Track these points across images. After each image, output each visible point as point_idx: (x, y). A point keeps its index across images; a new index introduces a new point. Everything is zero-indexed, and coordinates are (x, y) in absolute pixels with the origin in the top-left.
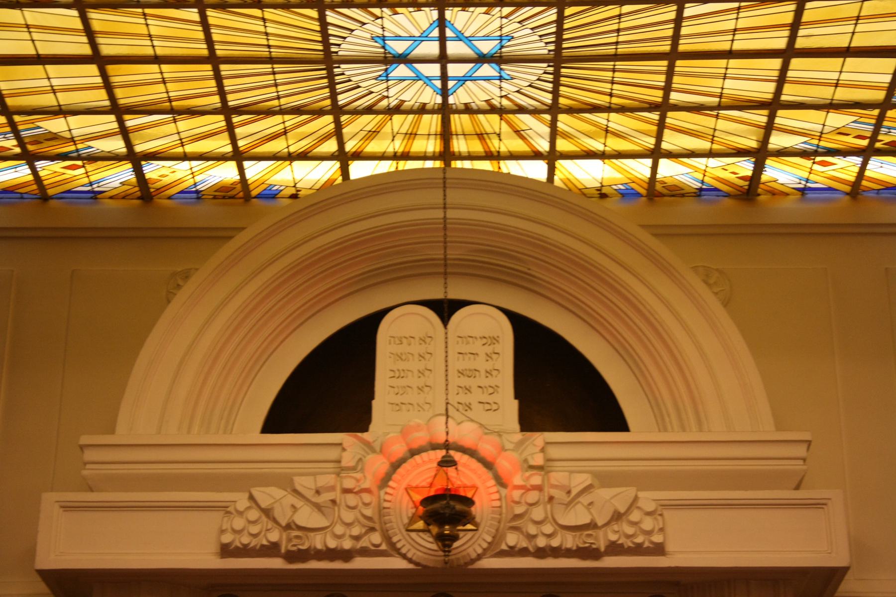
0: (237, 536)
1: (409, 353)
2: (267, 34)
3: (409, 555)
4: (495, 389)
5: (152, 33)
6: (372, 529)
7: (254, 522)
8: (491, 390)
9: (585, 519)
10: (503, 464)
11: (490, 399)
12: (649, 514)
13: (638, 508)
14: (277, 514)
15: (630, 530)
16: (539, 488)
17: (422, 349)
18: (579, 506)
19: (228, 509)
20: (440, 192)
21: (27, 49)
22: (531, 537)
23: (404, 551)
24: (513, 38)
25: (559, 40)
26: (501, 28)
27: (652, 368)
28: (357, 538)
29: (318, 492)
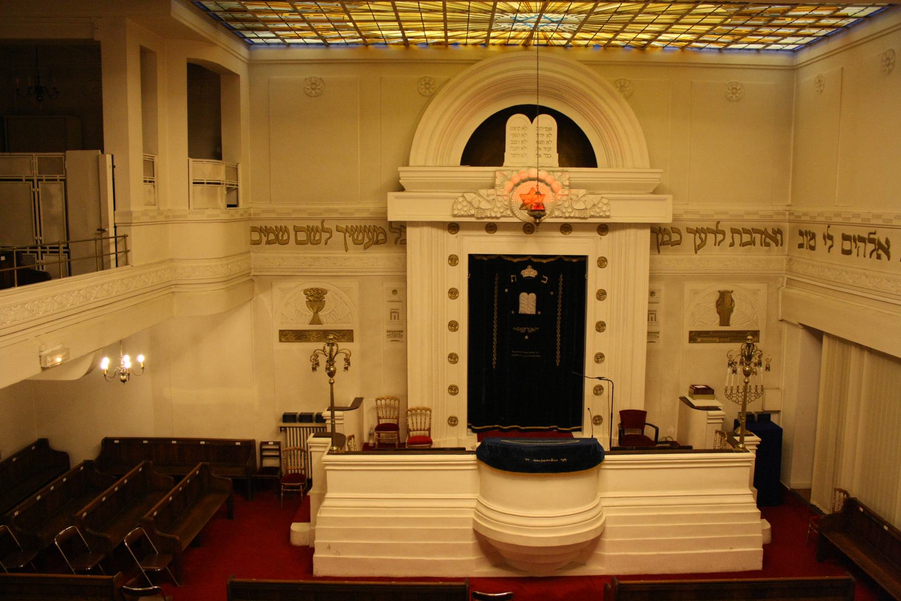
0: (459, 211)
1: (481, 60)
3: (520, 218)
4: (550, 149)
5: (421, 7)
7: (466, 206)
8: (548, 149)
9: (583, 207)
10: (555, 185)
11: (548, 153)
12: (605, 204)
13: (602, 202)
14: (473, 204)
15: (598, 211)
16: (567, 195)
17: (523, 132)
18: (581, 202)
20: (537, 71)
22: (563, 213)
23: (518, 217)
27: (606, 135)
29: (488, 196)
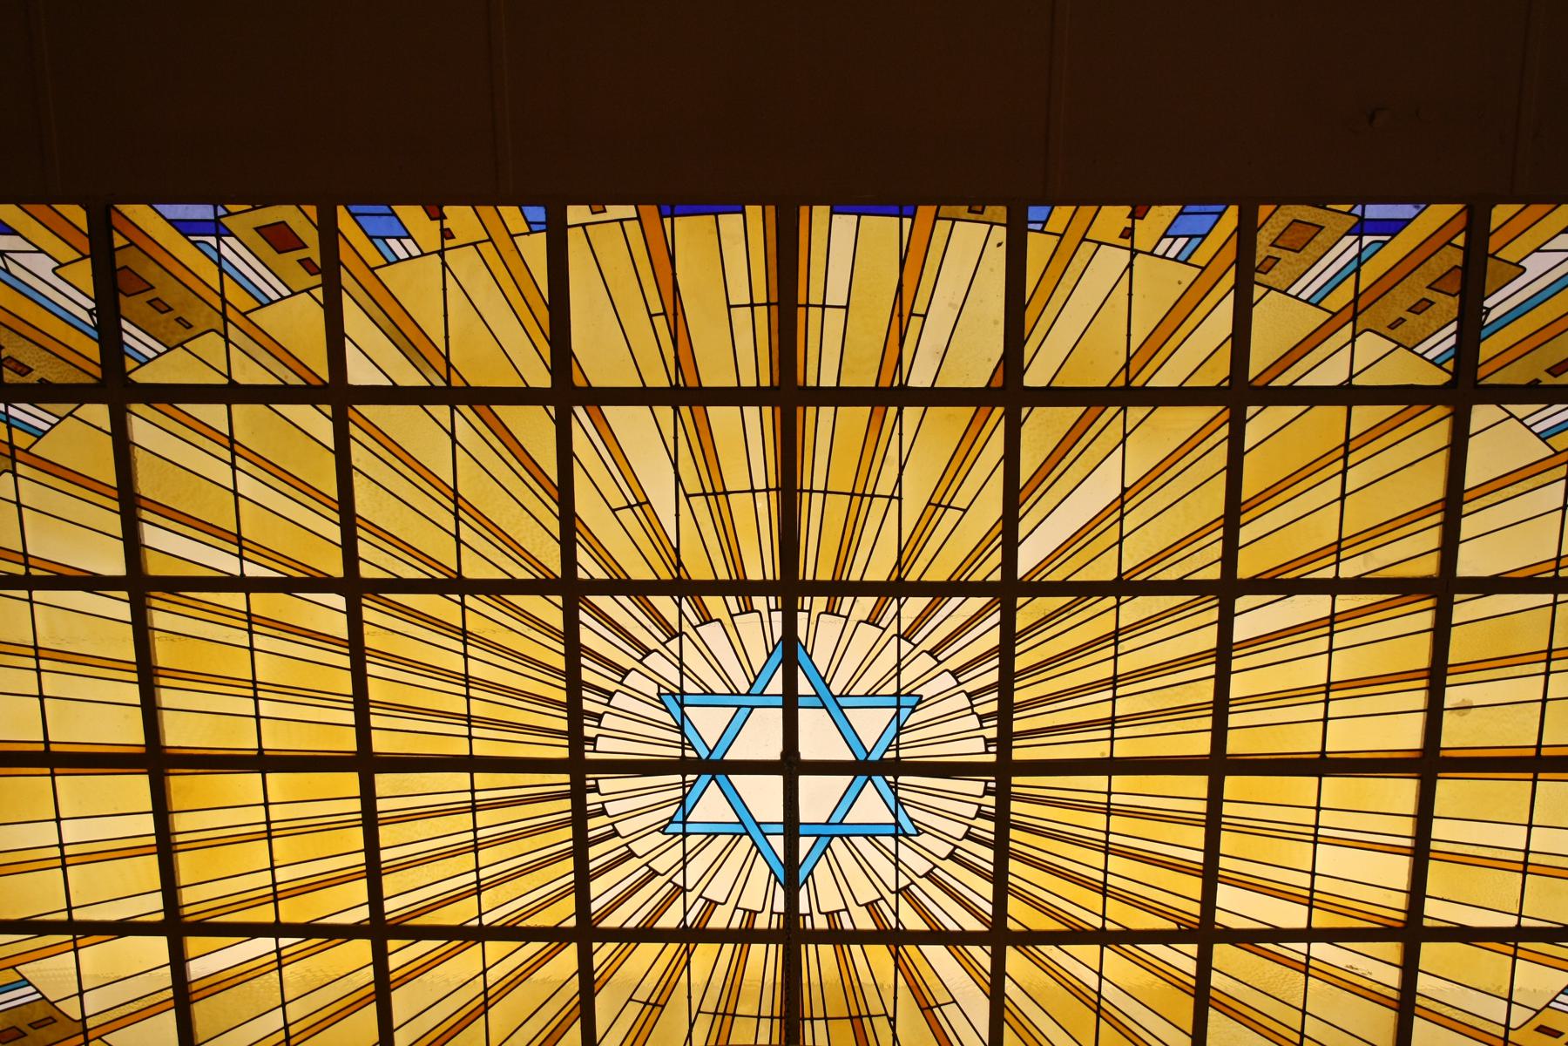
2: (467, 680)
21: (243, 739)
24: (663, 830)
25: (579, 818)
26: (684, 860)
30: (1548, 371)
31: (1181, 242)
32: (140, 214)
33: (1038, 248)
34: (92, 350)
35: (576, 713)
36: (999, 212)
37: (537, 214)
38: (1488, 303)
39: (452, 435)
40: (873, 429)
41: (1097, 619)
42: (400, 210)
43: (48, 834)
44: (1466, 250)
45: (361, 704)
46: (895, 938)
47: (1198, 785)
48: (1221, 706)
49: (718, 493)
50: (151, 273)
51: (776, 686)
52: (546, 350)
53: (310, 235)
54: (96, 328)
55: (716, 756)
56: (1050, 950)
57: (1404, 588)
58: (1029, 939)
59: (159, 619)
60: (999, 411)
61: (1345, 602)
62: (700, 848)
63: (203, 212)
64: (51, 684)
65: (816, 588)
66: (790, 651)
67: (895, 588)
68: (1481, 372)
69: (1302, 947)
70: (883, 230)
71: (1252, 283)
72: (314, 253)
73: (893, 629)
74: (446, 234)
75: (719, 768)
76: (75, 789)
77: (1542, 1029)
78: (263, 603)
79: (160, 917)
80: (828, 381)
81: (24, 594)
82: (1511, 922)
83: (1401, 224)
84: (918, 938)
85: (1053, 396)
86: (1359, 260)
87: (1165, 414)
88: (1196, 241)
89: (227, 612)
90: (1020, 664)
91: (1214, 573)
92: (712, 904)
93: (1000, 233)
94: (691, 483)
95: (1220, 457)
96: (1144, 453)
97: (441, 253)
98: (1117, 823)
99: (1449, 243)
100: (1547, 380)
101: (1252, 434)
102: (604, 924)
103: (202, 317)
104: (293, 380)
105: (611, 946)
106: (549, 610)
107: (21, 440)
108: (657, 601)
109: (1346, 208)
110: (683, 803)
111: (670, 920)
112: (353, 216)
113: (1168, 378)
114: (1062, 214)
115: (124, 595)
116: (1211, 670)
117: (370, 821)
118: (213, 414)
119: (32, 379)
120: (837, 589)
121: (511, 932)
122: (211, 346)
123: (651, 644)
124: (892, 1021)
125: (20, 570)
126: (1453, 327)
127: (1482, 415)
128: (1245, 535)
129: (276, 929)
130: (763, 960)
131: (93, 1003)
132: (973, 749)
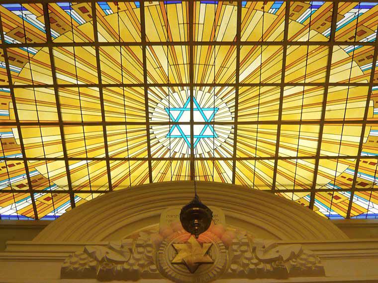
6: (152, 263)
19: (65, 261)
25: (148, 135)
28: (142, 266)
30: (349, 39)
31: (274, 10)
32: (53, 5)
33: (244, 11)
34: (45, 36)
35: (147, 112)
36: (236, 3)
37: (138, 4)
38: (337, 24)
39: (121, 53)
40: (209, 50)
41: (255, 91)
42: (109, 3)
43: (39, 140)
44: (333, 12)
45: (103, 111)
46: (213, 159)
47: (276, 127)
48: (280, 110)
49: (176, 65)
50: (56, 18)
51: (189, 106)
52: (140, 34)
53: (90, 9)
54: (45, 31)
55: (207, 125)
56: (244, 161)
57: (319, 85)
58: (240, 159)
59: (60, 94)
60: (236, 46)
61: (307, 88)
62: (173, 141)
63: (67, 4)
64: (39, 108)
65: (197, 85)
66: (192, 99)
67: (214, 85)
68: (335, 39)
69: (295, 160)
70: (212, 7)
71: (289, 19)
72: (91, 13)
73: (171, 151)
74: (119, 9)
75: (177, 124)
76: (44, 130)
77: (342, 177)
78: (82, 90)
79: (63, 157)
80: (200, 40)
81: (32, 89)
82: (337, 155)
83: (318, 7)
84: (218, 159)
85: (247, 43)
86: (311, 14)
87: (270, 47)
88: (277, 10)
89: (74, 92)
90: (239, 101)
91: (280, 82)
92: (176, 153)
93: (236, 8)
94: (171, 63)
95: (281, 57)
96: (266, 56)
97: (118, 13)
98: (259, 135)
99: (330, 10)
100: (349, 41)
101: (288, 52)
102: (233, 87)
103: (68, 28)
104: (87, 41)
105: (155, 161)
106: (141, 90)
107: (31, 56)
108: (219, 157)
109: (308, 3)
110: (170, 131)
111: (167, 156)
112: (99, 5)
113: (271, 39)
114: (249, 3)
115: (53, 88)
116: (279, 102)
117: (105, 136)
118: (70, 49)
119: (33, 42)
120: (202, 85)
121: (134, 159)
122: (69, 34)
123: (219, 148)
124: (213, 176)
125: (32, 84)
126: (330, 29)
127: (335, 48)
128: (286, 73)
129: (87, 159)
130: (186, 164)
131: (51, 175)
132: (230, 119)
